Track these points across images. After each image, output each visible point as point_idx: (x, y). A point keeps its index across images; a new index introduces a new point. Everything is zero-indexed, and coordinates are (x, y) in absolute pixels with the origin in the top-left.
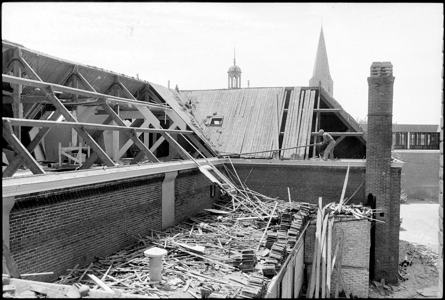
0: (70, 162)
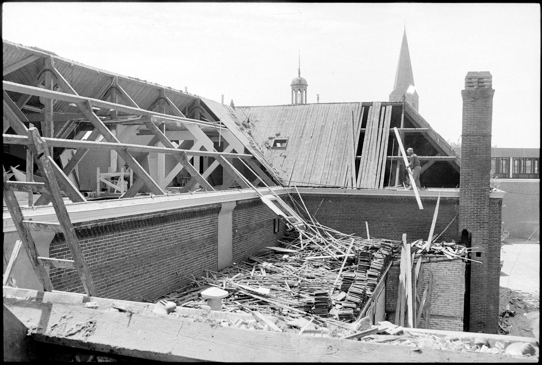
0: (109, 190)
